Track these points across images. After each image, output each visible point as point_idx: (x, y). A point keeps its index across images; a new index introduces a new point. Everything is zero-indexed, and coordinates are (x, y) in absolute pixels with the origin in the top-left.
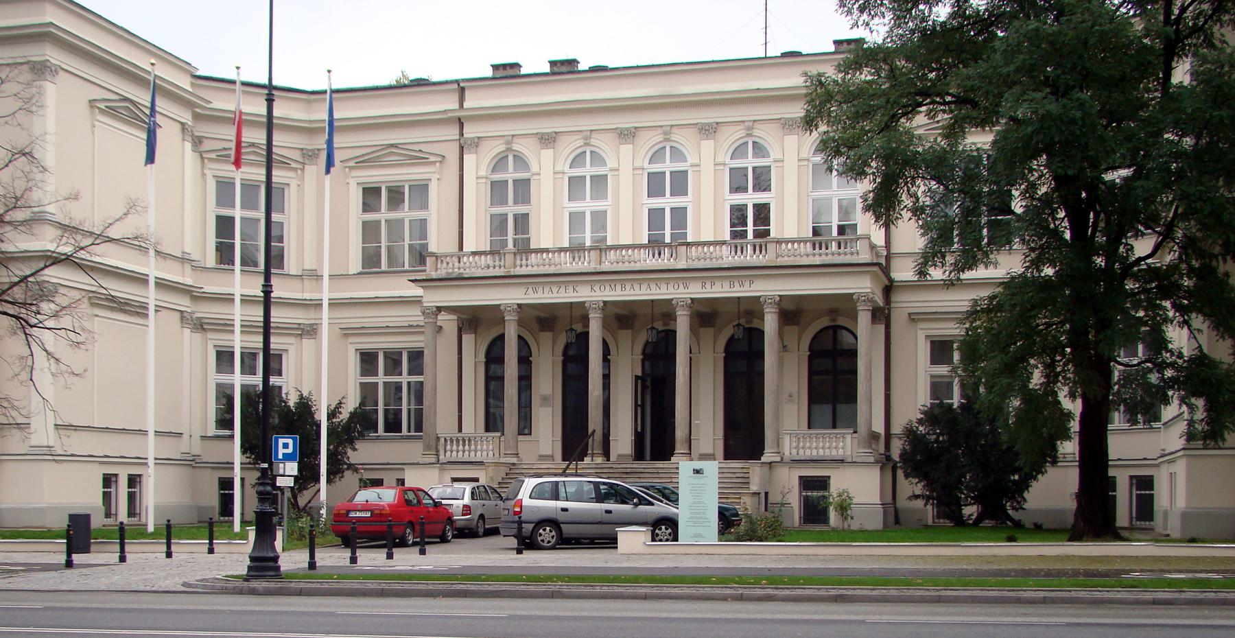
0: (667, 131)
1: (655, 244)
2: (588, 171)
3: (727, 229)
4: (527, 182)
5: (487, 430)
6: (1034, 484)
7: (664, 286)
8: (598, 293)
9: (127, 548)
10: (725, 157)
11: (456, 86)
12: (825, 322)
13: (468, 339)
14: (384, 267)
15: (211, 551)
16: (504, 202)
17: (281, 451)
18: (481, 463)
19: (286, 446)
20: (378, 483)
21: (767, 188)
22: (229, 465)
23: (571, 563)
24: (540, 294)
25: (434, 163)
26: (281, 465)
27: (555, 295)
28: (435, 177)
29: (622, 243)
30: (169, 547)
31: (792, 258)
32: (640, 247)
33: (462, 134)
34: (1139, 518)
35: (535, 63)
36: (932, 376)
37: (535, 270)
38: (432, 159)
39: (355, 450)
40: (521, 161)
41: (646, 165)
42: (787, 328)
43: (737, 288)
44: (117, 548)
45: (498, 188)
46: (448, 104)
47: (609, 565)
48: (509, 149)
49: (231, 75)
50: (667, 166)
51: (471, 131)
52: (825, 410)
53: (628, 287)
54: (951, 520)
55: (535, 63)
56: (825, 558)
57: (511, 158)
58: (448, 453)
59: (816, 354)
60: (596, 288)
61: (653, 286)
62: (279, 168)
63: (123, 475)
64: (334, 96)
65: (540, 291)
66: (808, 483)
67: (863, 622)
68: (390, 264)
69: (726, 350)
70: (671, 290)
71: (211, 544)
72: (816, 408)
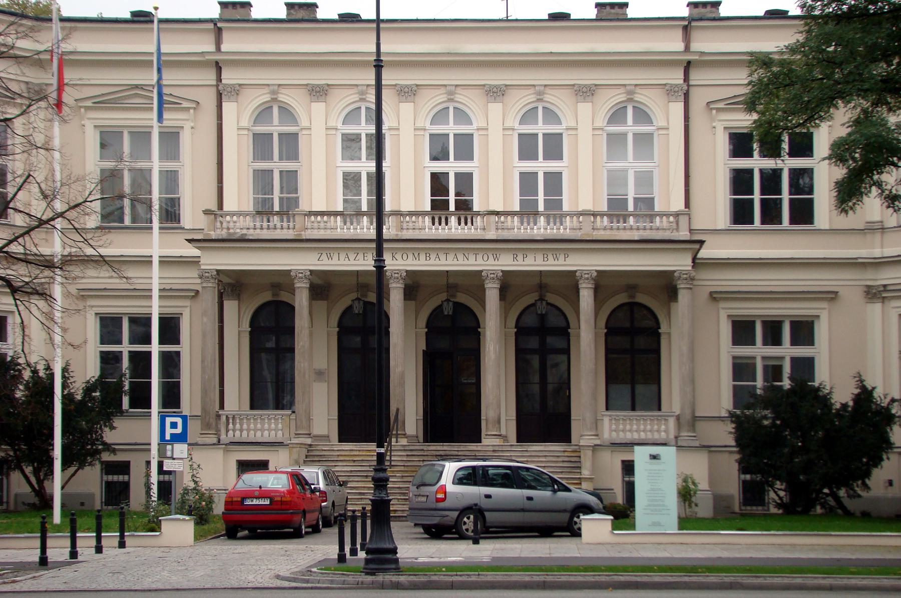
0: (451, 91)
1: (528, 212)
4: (295, 136)
5: (252, 407)
6: (876, 472)
9: (50, 543)
10: (601, 122)
11: (211, 26)
12: (267, 297)
13: (230, 307)
14: (127, 221)
15: (122, 545)
16: (269, 157)
17: (169, 431)
18: (280, 444)
19: (174, 425)
20: (262, 466)
23: (526, 554)
24: (335, 261)
25: (187, 109)
26: (169, 447)
27: (352, 262)
28: (187, 126)
29: (315, 209)
30: (99, 539)
31: (608, 232)
33: (219, 79)
36: (734, 358)
37: (636, 236)
38: (185, 104)
39: (112, 428)
40: (287, 113)
41: (428, 126)
42: (314, 302)
44: (68, 542)
45: (261, 144)
47: (442, 560)
48: (274, 100)
51: (230, 77)
54: (800, 509)
57: (276, 110)
58: (231, 433)
59: (345, 330)
61: (460, 256)
62: (169, 109)
64: (163, 26)
65: (335, 257)
68: (134, 220)
69: (340, 325)
71: (122, 536)
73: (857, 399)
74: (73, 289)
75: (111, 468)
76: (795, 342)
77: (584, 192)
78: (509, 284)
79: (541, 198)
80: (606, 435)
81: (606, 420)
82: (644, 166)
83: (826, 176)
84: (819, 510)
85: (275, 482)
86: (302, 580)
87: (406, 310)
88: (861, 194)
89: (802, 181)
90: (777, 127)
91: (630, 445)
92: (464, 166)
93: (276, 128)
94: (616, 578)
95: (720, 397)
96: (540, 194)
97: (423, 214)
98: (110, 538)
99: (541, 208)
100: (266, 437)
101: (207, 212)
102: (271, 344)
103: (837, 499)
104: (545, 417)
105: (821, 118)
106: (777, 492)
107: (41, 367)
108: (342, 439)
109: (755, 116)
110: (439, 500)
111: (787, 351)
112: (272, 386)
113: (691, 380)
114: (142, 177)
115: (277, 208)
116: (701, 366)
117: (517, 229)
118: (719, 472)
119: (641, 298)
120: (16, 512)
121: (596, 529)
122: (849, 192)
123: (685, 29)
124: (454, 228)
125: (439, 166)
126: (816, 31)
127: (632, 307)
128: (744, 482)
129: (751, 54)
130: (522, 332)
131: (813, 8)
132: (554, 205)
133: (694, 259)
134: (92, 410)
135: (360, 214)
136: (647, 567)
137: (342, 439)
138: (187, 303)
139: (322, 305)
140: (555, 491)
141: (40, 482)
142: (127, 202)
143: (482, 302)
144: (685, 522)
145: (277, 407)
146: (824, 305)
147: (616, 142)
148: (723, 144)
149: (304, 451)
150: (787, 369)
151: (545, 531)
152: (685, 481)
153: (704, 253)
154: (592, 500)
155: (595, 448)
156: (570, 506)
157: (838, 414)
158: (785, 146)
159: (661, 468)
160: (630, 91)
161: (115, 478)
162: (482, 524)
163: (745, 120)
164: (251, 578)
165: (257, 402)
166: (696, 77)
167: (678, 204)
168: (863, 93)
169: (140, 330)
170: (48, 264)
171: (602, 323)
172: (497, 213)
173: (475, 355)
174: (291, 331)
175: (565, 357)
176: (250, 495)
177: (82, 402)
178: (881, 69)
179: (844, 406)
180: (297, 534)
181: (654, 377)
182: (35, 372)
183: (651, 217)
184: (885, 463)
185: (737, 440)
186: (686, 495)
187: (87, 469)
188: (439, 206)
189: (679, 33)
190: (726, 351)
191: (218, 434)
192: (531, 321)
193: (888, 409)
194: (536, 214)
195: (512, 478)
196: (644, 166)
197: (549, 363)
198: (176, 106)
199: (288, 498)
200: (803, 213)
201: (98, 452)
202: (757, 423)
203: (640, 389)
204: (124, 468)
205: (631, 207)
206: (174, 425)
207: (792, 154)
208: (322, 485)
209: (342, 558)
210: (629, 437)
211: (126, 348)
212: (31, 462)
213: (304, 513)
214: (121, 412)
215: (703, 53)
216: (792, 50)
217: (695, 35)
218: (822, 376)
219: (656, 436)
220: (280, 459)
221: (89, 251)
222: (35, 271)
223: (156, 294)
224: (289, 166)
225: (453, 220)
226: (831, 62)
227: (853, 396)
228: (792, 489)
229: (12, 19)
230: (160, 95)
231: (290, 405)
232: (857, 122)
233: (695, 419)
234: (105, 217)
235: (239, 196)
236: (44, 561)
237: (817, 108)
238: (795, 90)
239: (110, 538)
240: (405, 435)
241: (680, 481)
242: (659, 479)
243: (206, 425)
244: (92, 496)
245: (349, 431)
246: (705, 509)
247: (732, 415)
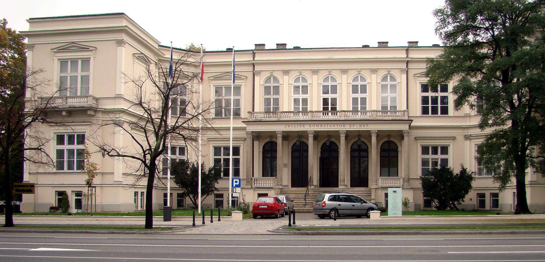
1: (355, 111)
3: (322, 106)
5: (263, 176)
6: (466, 196)
7: (336, 126)
8: (312, 128)
9: (196, 219)
10: (379, 80)
12: (268, 140)
13: (256, 143)
14: (223, 116)
15: (219, 220)
17: (235, 184)
18: (272, 188)
19: (236, 182)
20: (266, 195)
21: (307, 93)
24: (291, 128)
28: (243, 84)
29: (284, 111)
30: (212, 218)
33: (254, 69)
34: (493, 207)
35: (271, 45)
37: (390, 118)
38: (243, 78)
39: (218, 183)
40: (276, 80)
41: (322, 83)
43: (362, 127)
44: (202, 219)
45: (267, 90)
49: (169, 45)
50: (359, 83)
51: (257, 68)
52: (386, 170)
53: (323, 125)
54: (442, 208)
55: (271, 45)
56: (445, 221)
57: (272, 79)
59: (293, 151)
60: (312, 126)
61: (332, 126)
67: (207, 240)
68: (225, 115)
69: (292, 149)
70: (339, 127)
71: (219, 217)
73: (461, 172)
74: (205, 139)
75: (217, 196)
77: (374, 104)
78: (348, 135)
79: (359, 106)
80: (380, 185)
81: (380, 180)
82: (393, 95)
83: (452, 98)
84: (448, 209)
85: (269, 200)
86: (276, 232)
87: (314, 143)
88: (462, 104)
89: (444, 100)
90: (436, 82)
91: (387, 188)
92: (334, 96)
93: (272, 84)
94: (380, 231)
96: (359, 105)
97: (320, 112)
98: (215, 218)
99: (359, 109)
101: (249, 112)
102: (269, 156)
103: (454, 205)
104: (360, 179)
105: (450, 80)
106: (435, 203)
107: (195, 164)
108: (293, 186)
109: (429, 79)
110: (323, 206)
111: (439, 156)
112: (269, 169)
113: (408, 166)
114: (228, 102)
115: (272, 111)
116: (412, 162)
117: (351, 116)
118: (416, 197)
119: (392, 139)
120: (187, 209)
121: (375, 215)
122: (458, 104)
123: (407, 50)
124: (330, 116)
125: (326, 96)
126: (448, 50)
127: (389, 142)
128: (425, 200)
129: (427, 58)
130: (352, 151)
131: (446, 43)
132: (364, 108)
133: (410, 126)
134: (211, 177)
135: (299, 112)
136: (390, 227)
137: (293, 186)
138: (242, 142)
139: (286, 142)
140: (362, 203)
141: (195, 200)
142: (223, 110)
143: (340, 142)
144: (404, 213)
145: (271, 176)
146: (451, 141)
147: (384, 87)
148: (419, 88)
149: (280, 191)
150: (439, 163)
151: (359, 216)
152: (405, 199)
153: (413, 124)
154: (374, 206)
155: (376, 189)
156: (367, 208)
157: (455, 177)
158: (439, 89)
159: (397, 195)
160: (389, 70)
161: (219, 199)
162: (337, 214)
163: (425, 80)
164: (259, 231)
166: (411, 66)
167: (404, 108)
168: (463, 71)
169: (227, 152)
170: (196, 130)
171: (379, 148)
172: (344, 111)
174: (276, 151)
175: (366, 159)
176: (261, 204)
177: (208, 175)
178: (468, 64)
179: (457, 174)
180: (276, 217)
181: (396, 165)
182: (194, 165)
183: (396, 112)
184: (469, 193)
185: (422, 186)
186: (405, 204)
187: (210, 196)
188: (325, 109)
189: (405, 52)
190: (420, 156)
191: (251, 185)
192: (356, 147)
193: (471, 175)
194: (358, 111)
195: (348, 199)
196: (393, 95)
197: (361, 161)
198: (240, 78)
199: (273, 206)
200: (445, 111)
201: (213, 191)
202: (429, 180)
203: (391, 169)
204: (221, 196)
205: (389, 109)
206: (236, 182)
207: (441, 91)
208: (285, 202)
209: (290, 225)
210: (387, 185)
211: (222, 157)
212: (192, 194)
213: (279, 210)
214: (220, 178)
215: (412, 58)
216: (441, 57)
217: (410, 52)
218: (450, 165)
219: (396, 185)
220: (272, 193)
221: (209, 126)
222: (191, 132)
223: (231, 139)
224: (276, 97)
225: (330, 114)
226: (453, 61)
228: (440, 201)
229: (186, 52)
230: (234, 75)
231: (276, 176)
232: (461, 81)
233: (409, 179)
234: (217, 114)
235: (259, 107)
236: (194, 225)
237: (448, 76)
238: (441, 70)
239: (215, 218)
240: (313, 185)
241: (403, 200)
242: (396, 199)
243: (248, 182)
244: (211, 204)
245: (295, 184)
246: (411, 209)
247: (421, 178)
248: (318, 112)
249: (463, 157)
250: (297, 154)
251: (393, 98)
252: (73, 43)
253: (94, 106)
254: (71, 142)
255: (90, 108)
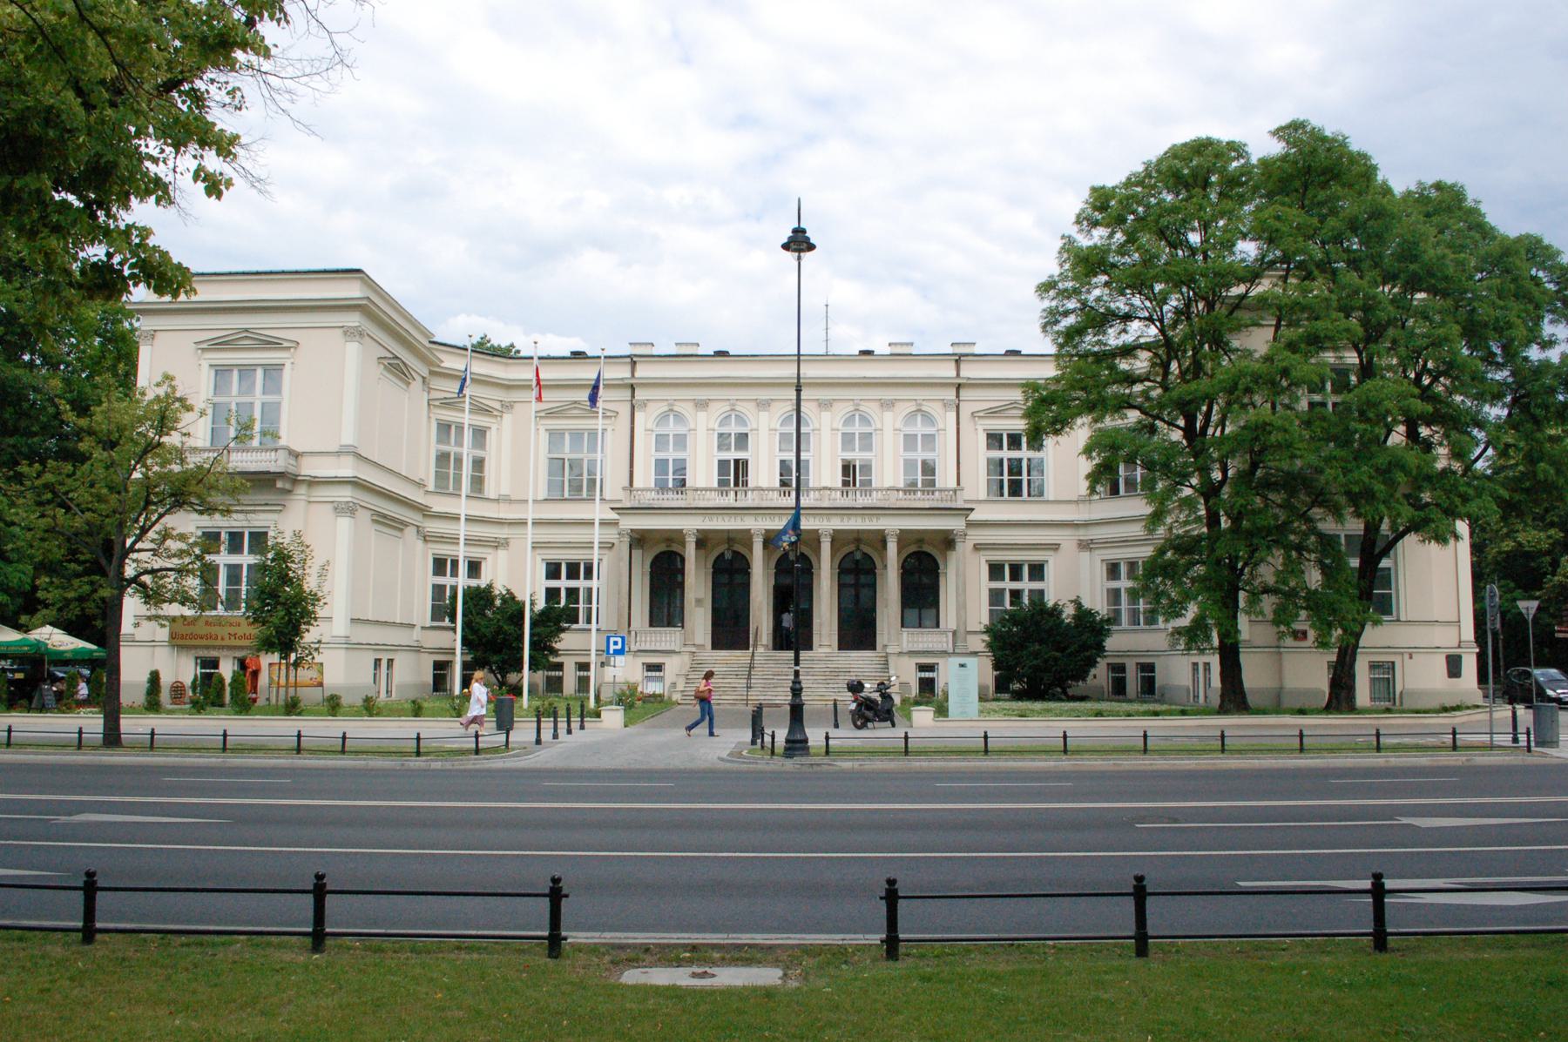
1: (911, 488)
2: (857, 428)
3: (778, 478)
12: (662, 548)
17: (612, 647)
18: (673, 652)
19: (616, 643)
22: (452, 651)
32: (711, 490)
35: (881, 348)
45: (661, 441)
46: (947, 371)
51: (640, 394)
52: (912, 614)
63: (385, 658)
66: (923, 668)
72: (908, 612)
76: (1031, 579)
95: (980, 615)
100: (938, 647)
116: (968, 596)
165: (654, 621)
166: (964, 394)
171: (773, 564)
173: (746, 586)
189: (953, 365)
190: (982, 585)
192: (849, 565)
206: (616, 643)
217: (962, 366)
218: (1050, 601)
223: (596, 545)
227: (321, 612)
235: (645, 477)
247: (988, 630)
248: (769, 490)
249: (1075, 583)
250: (724, 579)
251: (897, 462)
252: (246, 330)
253: (292, 469)
254: (235, 548)
255: (281, 475)
